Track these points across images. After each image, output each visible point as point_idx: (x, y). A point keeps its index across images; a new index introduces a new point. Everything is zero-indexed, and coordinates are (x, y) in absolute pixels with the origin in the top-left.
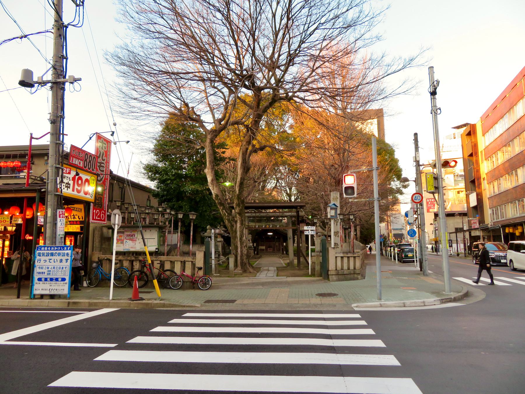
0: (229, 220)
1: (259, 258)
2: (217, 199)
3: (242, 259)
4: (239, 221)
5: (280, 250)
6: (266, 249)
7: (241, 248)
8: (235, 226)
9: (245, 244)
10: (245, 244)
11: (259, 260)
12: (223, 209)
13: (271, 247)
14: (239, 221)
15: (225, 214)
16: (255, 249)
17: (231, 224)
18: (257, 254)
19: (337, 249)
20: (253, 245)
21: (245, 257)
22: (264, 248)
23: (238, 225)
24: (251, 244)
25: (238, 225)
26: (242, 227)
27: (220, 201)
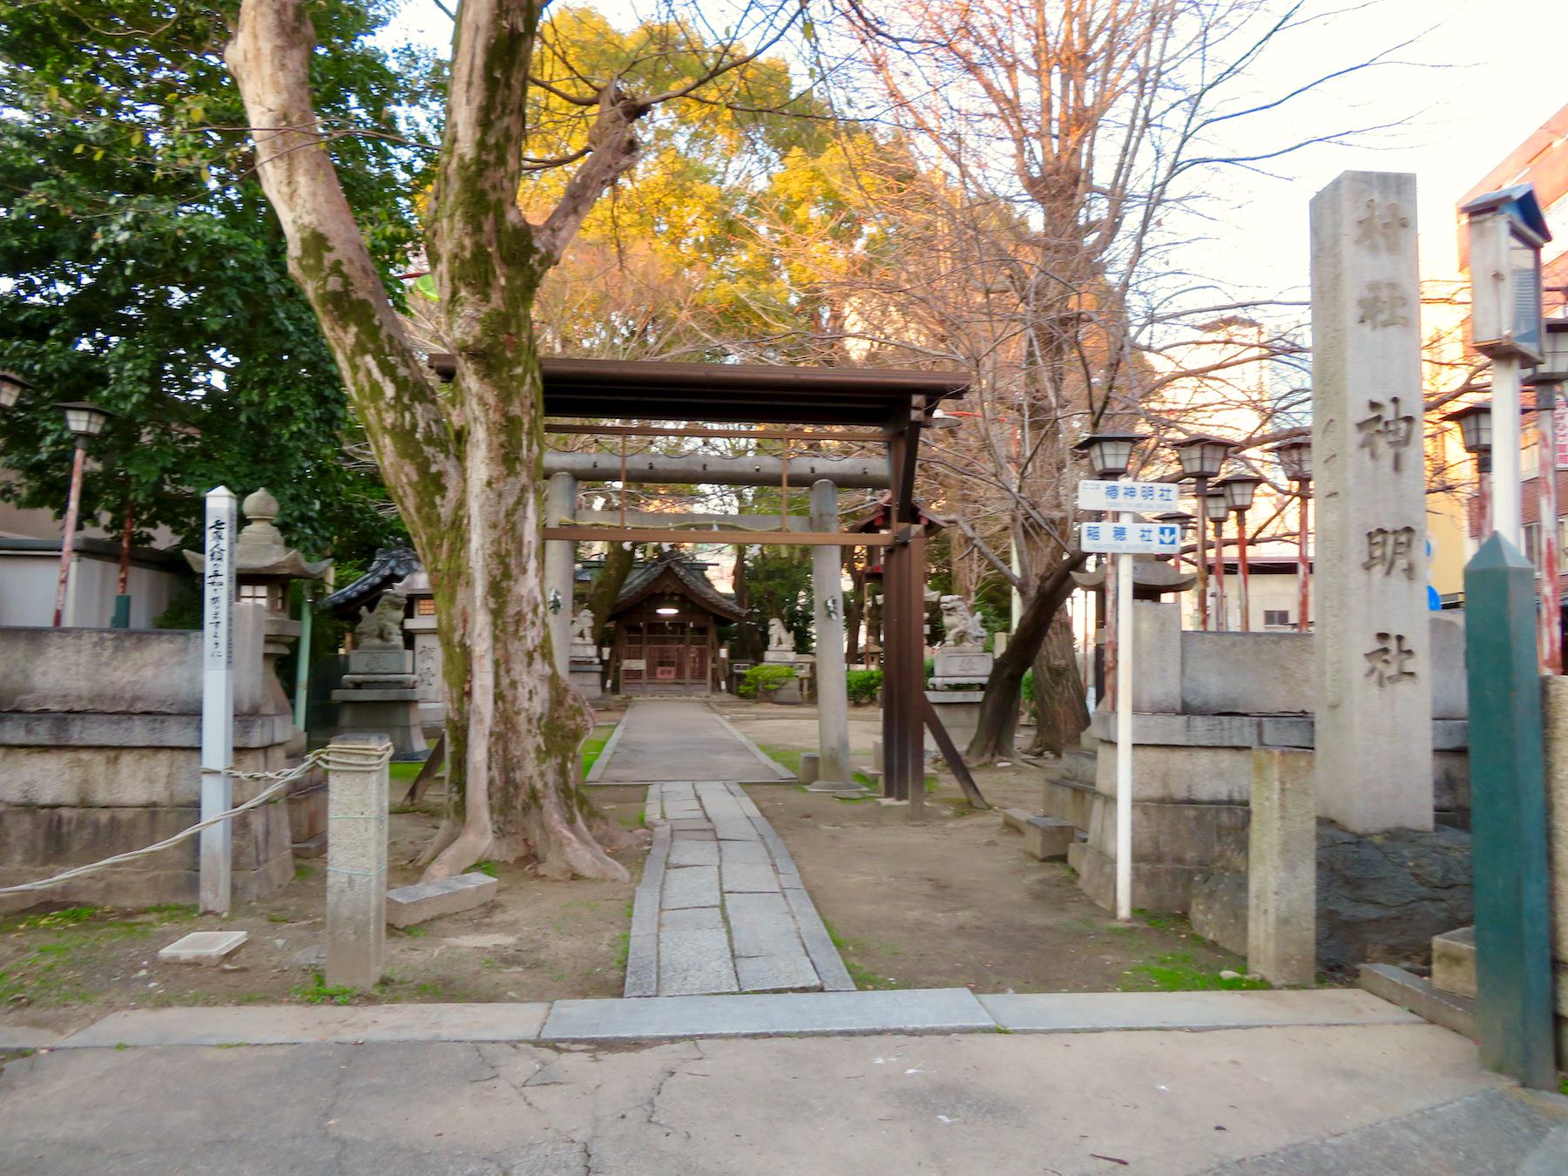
0: (404, 437)
1: (624, 706)
2: (313, 270)
3: (504, 762)
4: (479, 434)
5: (702, 675)
6: (651, 671)
7: (501, 665)
8: (452, 482)
9: (532, 637)
10: (532, 637)
11: (626, 718)
12: (360, 348)
13: (671, 664)
14: (479, 434)
15: (377, 391)
16: (608, 670)
17: (423, 466)
18: (615, 689)
19: (1404, 687)
20: (600, 655)
21: (530, 743)
22: (641, 665)
23: (479, 465)
24: (591, 651)
25: (479, 465)
26: (511, 487)
27: (334, 284)
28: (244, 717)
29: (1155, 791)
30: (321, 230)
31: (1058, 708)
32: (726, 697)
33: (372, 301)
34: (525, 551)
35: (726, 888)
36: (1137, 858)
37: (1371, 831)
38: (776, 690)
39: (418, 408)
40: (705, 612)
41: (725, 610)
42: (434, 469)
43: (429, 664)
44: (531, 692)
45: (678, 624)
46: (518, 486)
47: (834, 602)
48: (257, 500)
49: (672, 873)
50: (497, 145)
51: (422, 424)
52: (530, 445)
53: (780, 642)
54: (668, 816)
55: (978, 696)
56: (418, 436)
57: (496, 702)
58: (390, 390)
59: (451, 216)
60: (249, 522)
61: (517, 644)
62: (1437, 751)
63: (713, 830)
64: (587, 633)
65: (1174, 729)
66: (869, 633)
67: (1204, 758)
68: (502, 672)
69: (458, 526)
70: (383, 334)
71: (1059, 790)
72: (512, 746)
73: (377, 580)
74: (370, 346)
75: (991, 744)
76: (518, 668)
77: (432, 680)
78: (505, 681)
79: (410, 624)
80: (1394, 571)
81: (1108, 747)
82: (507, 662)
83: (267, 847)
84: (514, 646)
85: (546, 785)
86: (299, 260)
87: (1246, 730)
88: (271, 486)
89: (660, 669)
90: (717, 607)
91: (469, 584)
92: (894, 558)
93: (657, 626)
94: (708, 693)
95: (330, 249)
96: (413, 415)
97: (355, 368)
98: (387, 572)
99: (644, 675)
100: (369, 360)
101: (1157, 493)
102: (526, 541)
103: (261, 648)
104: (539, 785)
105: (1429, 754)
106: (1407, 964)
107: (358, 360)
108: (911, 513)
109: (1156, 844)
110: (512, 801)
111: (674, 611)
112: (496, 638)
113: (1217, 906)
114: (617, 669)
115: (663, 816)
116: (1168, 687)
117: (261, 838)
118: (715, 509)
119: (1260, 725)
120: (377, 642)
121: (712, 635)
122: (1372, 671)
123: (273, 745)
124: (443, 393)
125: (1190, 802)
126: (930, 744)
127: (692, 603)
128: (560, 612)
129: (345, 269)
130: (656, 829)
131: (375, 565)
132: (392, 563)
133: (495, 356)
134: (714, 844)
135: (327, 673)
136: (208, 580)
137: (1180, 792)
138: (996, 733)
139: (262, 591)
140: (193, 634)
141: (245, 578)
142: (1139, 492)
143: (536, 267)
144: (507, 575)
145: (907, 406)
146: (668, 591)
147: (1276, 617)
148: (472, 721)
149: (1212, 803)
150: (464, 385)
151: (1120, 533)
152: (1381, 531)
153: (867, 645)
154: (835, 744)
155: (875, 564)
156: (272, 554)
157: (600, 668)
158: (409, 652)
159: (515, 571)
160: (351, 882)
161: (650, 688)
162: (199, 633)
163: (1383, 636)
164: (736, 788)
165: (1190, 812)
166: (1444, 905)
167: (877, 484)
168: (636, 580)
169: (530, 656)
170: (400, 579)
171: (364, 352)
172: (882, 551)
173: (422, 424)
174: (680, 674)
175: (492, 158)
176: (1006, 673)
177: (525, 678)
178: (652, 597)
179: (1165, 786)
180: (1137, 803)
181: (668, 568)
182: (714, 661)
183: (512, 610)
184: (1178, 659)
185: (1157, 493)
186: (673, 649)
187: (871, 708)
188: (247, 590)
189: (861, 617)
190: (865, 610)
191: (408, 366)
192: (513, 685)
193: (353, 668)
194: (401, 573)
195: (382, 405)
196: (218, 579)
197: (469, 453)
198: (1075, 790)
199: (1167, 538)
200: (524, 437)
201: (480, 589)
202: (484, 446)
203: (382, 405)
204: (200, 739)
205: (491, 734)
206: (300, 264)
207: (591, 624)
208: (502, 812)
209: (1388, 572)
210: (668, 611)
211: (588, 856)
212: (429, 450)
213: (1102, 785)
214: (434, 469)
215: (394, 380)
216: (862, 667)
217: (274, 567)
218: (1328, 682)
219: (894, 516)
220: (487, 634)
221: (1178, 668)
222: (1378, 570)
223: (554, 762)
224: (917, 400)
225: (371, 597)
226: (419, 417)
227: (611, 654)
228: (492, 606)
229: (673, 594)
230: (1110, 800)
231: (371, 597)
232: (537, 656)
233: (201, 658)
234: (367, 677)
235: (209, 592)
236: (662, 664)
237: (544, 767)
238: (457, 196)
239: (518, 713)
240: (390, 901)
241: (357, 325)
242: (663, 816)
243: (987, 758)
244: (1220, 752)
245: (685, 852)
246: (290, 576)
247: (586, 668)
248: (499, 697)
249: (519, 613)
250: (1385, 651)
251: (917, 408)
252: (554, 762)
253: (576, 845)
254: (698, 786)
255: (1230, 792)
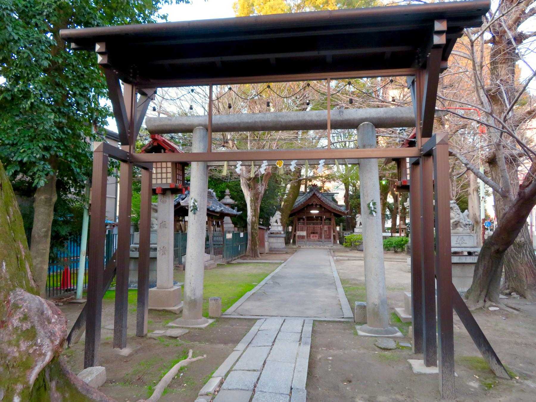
1: (294, 251)
5: (330, 238)
6: (308, 235)
11: (292, 256)
22: (304, 233)
31: (520, 267)
32: (339, 247)
38: (359, 245)
40: (329, 211)
41: (338, 211)
45: (318, 218)
47: (374, 204)
64: (279, 221)
66: (401, 220)
75: (483, 294)
89: (312, 235)
90: (335, 210)
92: (419, 169)
93: (311, 218)
94: (332, 245)
99: (306, 237)
111: (317, 212)
114: (295, 236)
121: (333, 221)
126: (459, 327)
127: (325, 208)
128: (198, 213)
138: (487, 284)
145: (430, 32)
146: (314, 203)
153: (400, 225)
155: (403, 179)
161: (308, 243)
168: (300, 200)
174: (320, 237)
176: (493, 249)
178: (308, 206)
181: (314, 194)
182: (334, 232)
186: (318, 227)
187: (402, 254)
189: (397, 213)
190: (399, 210)
210: (315, 212)
216: (398, 235)
224: (440, 26)
227: (292, 229)
229: (316, 205)
236: (314, 233)
243: (481, 302)
247: (278, 235)
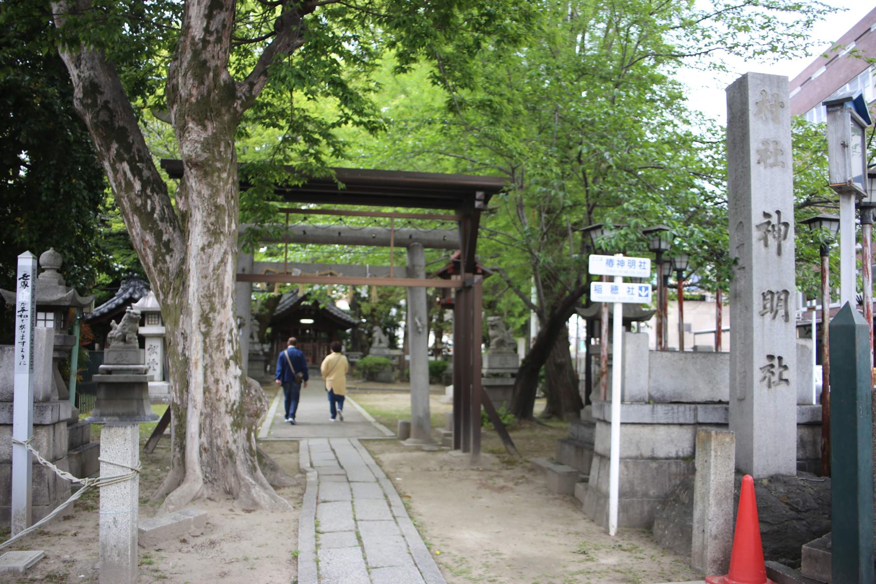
8: (177, 246)
14: (198, 216)
19: (783, 387)
27: (104, 116)
28: (39, 403)
29: (634, 453)
30: (96, 80)
33: (128, 127)
34: (225, 294)
35: (357, 517)
36: (622, 495)
37: (761, 477)
39: (156, 198)
42: (165, 238)
43: (154, 356)
44: (227, 386)
46: (223, 251)
48: (47, 256)
49: (321, 506)
50: (217, 31)
51: (158, 208)
52: (230, 223)
53: (380, 342)
54: (315, 464)
55: (512, 382)
56: (155, 216)
57: (204, 393)
58: (138, 186)
59: (185, 75)
60: (43, 270)
61: (218, 354)
62: (798, 424)
63: (346, 475)
65: (644, 413)
67: (662, 430)
68: (209, 373)
69: (182, 274)
70: (134, 150)
71: (567, 447)
72: (215, 423)
73: (121, 301)
74: (126, 156)
76: (220, 370)
77: (156, 367)
78: (211, 380)
79: (143, 331)
80: (777, 317)
81: (603, 425)
82: (212, 366)
83: (55, 489)
84: (217, 356)
85: (238, 447)
86: (81, 101)
87: (688, 413)
88: (56, 246)
91: (189, 314)
95: (102, 93)
96: (153, 202)
97: (115, 171)
98: (127, 295)
100: (126, 166)
101: (638, 264)
102: (225, 287)
103: (51, 354)
104: (234, 448)
105: (796, 425)
106: (783, 560)
107: (118, 166)
108: (472, 267)
109: (632, 484)
110: (217, 460)
112: (205, 350)
113: (671, 525)
115: (312, 466)
116: (642, 385)
117: (51, 484)
118: (339, 261)
119: (696, 410)
120: (121, 344)
122: (765, 378)
123: (59, 422)
124: (172, 184)
125: (653, 459)
129: (110, 106)
130: (308, 474)
131: (120, 291)
132: (131, 290)
133: (209, 165)
134: (347, 485)
135: (89, 367)
136: (17, 314)
137: (647, 453)
139: (50, 316)
140: (7, 348)
141: (41, 307)
142: (626, 263)
143: (239, 109)
144: (213, 309)
147: (604, 279)
148: (190, 406)
149: (667, 459)
150: (188, 184)
151: (615, 290)
152: (771, 292)
154: (421, 414)
156: (59, 294)
157: (264, 358)
158: (142, 350)
159: (218, 307)
160: (115, 521)
162: (10, 347)
163: (770, 357)
164: (356, 443)
165: (654, 465)
166: (804, 522)
167: (450, 247)
169: (227, 364)
170: (136, 301)
171: (122, 160)
172: (453, 290)
173: (158, 208)
175: (212, 39)
177: (224, 377)
179: (638, 448)
180: (622, 459)
183: (215, 332)
184: (647, 369)
185: (638, 264)
188: (41, 316)
191: (150, 169)
192: (217, 381)
193: (105, 361)
194: (136, 296)
195: (133, 195)
196: (25, 313)
197: (191, 230)
198: (577, 447)
199: (643, 293)
200: (226, 218)
201: (195, 317)
202: (200, 225)
203: (133, 195)
204: (12, 419)
205: (201, 414)
206: (81, 102)
207: (258, 329)
208: (208, 464)
209: (774, 318)
211: (266, 496)
212: (161, 226)
213: (599, 447)
214: (165, 238)
215: (141, 179)
217: (60, 300)
218: (737, 384)
219: (462, 269)
220: (200, 346)
221: (647, 374)
222: (769, 316)
223: (243, 432)
224: (479, 194)
225: (117, 313)
226: (156, 203)
228: (203, 330)
230: (605, 458)
231: (117, 313)
232: (231, 362)
233: (13, 364)
234: (115, 366)
235: (18, 322)
237: (236, 436)
238: (189, 63)
239: (219, 400)
240: (141, 532)
241: (117, 142)
242: (312, 466)
244: (672, 427)
245: (330, 490)
246: (68, 307)
248: (206, 390)
249: (220, 334)
250: (772, 366)
251: (479, 200)
252: (243, 432)
253: (258, 488)
254: (333, 442)
255: (677, 452)
